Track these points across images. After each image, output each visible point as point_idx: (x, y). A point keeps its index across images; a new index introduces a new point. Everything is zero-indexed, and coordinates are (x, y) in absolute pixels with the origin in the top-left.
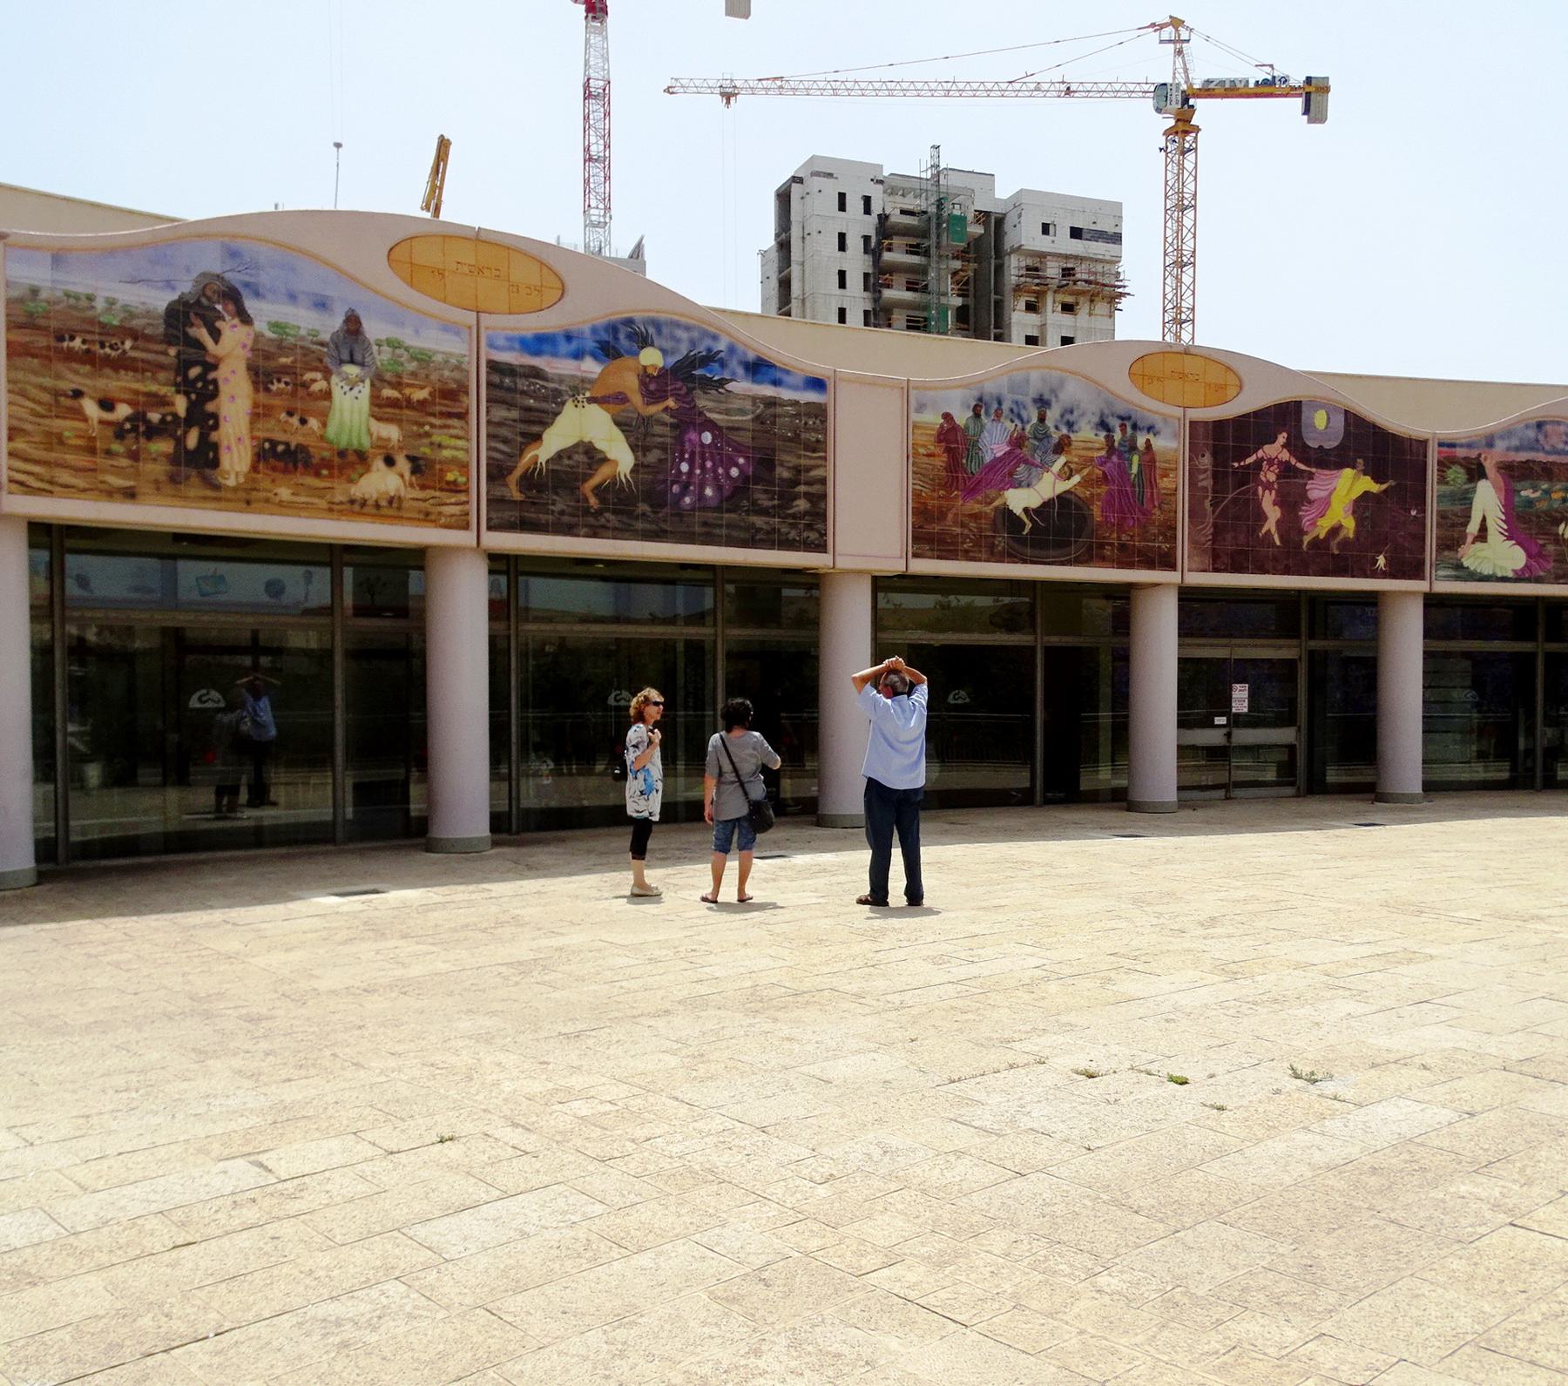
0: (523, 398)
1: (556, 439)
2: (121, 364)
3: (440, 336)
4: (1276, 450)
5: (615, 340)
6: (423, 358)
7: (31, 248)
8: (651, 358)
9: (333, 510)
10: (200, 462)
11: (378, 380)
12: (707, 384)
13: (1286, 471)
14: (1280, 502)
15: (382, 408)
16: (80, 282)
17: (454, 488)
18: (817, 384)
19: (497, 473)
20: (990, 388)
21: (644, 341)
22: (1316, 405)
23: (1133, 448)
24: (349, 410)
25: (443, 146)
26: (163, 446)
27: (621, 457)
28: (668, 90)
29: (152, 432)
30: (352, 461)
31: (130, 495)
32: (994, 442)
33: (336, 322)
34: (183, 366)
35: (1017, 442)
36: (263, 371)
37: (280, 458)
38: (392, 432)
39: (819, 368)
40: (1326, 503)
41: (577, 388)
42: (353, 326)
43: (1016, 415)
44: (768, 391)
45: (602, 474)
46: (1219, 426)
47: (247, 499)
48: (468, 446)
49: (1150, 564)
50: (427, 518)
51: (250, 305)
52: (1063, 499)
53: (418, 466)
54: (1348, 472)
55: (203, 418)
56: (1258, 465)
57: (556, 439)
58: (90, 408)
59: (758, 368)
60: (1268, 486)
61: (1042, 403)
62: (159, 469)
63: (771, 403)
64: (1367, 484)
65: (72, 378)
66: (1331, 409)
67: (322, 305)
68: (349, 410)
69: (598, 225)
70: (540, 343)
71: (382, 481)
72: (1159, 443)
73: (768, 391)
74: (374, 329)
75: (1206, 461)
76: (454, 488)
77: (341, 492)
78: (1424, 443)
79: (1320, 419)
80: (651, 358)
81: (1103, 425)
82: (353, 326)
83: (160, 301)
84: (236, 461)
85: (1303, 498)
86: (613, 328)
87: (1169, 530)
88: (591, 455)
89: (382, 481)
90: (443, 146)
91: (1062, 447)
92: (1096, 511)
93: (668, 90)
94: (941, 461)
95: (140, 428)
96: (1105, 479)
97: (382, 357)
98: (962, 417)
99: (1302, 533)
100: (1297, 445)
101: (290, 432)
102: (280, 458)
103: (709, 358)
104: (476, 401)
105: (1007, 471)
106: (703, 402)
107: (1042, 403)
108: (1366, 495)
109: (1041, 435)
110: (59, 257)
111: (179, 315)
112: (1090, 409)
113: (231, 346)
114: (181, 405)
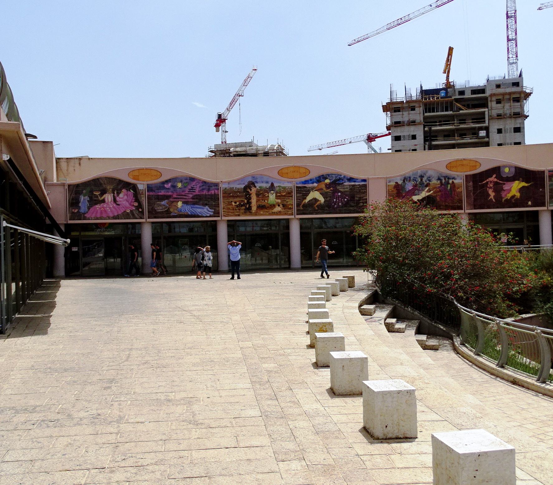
0: (303, 191)
1: (309, 198)
2: (237, 196)
3: (288, 184)
4: (493, 178)
5: (320, 179)
6: (284, 188)
7: (225, 182)
8: (327, 181)
9: (270, 214)
10: (248, 210)
11: (277, 193)
12: (339, 184)
13: (496, 184)
14: (494, 191)
15: (277, 197)
16: (232, 186)
17: (290, 209)
18: (364, 180)
19: (298, 205)
20: (407, 175)
21: (326, 178)
22: (505, 167)
23: (448, 183)
24: (272, 198)
25: (451, 49)
26: (244, 208)
27: (322, 200)
28: (540, 9)
29: (242, 206)
30: (273, 206)
31: (239, 215)
32: (409, 186)
33: (270, 185)
34: (246, 195)
35: (415, 186)
36: (258, 195)
37: (261, 207)
38: (279, 201)
39: (363, 177)
40: (510, 190)
41: (313, 189)
42: (272, 184)
43: (415, 180)
44: (353, 183)
45: (318, 203)
46: (474, 176)
47: (256, 214)
48: (293, 201)
49: (455, 209)
50: (286, 214)
51: (256, 185)
52: (428, 197)
53: (284, 206)
54: (517, 182)
55: (249, 203)
56: (487, 183)
57: (309, 198)
58: (233, 204)
59: (351, 179)
60: (490, 188)
61: (422, 177)
62: (243, 211)
63: (353, 186)
64: (524, 184)
65: (231, 200)
66: (510, 167)
67: (267, 182)
68: (272, 198)
69: (513, 63)
70: (306, 182)
71: (278, 209)
72: (456, 181)
73: (353, 183)
74: (276, 185)
75: (471, 184)
76: (290, 209)
77: (271, 211)
78: (543, 172)
79: (507, 170)
80: (327, 181)
81: (439, 179)
82: (272, 184)
83: (243, 186)
84: (254, 208)
85: (502, 189)
86: (319, 177)
87: (460, 201)
88: (316, 200)
89: (278, 209)
90: (451, 49)
91: (427, 185)
92: (438, 199)
93: (540, 9)
94: (395, 192)
95: (240, 205)
96: (440, 191)
97: (277, 189)
98: (400, 182)
99: (502, 198)
100: (499, 177)
101: (262, 203)
102: (261, 207)
103: (340, 179)
104: (294, 194)
105: (413, 192)
106: (338, 187)
107: (422, 177)
108: (523, 187)
109: (421, 183)
110: (229, 183)
111: (245, 188)
112: (435, 175)
113: (253, 191)
114: (246, 201)
